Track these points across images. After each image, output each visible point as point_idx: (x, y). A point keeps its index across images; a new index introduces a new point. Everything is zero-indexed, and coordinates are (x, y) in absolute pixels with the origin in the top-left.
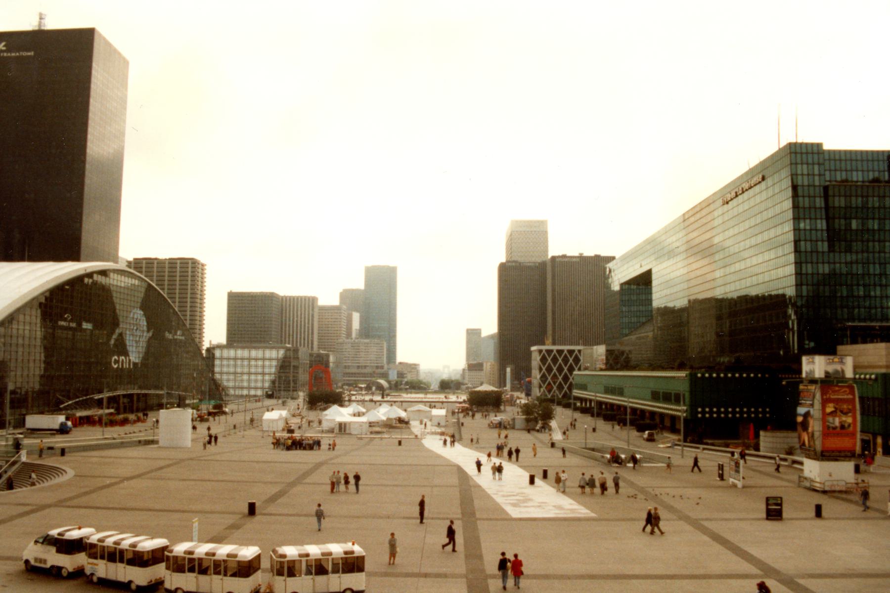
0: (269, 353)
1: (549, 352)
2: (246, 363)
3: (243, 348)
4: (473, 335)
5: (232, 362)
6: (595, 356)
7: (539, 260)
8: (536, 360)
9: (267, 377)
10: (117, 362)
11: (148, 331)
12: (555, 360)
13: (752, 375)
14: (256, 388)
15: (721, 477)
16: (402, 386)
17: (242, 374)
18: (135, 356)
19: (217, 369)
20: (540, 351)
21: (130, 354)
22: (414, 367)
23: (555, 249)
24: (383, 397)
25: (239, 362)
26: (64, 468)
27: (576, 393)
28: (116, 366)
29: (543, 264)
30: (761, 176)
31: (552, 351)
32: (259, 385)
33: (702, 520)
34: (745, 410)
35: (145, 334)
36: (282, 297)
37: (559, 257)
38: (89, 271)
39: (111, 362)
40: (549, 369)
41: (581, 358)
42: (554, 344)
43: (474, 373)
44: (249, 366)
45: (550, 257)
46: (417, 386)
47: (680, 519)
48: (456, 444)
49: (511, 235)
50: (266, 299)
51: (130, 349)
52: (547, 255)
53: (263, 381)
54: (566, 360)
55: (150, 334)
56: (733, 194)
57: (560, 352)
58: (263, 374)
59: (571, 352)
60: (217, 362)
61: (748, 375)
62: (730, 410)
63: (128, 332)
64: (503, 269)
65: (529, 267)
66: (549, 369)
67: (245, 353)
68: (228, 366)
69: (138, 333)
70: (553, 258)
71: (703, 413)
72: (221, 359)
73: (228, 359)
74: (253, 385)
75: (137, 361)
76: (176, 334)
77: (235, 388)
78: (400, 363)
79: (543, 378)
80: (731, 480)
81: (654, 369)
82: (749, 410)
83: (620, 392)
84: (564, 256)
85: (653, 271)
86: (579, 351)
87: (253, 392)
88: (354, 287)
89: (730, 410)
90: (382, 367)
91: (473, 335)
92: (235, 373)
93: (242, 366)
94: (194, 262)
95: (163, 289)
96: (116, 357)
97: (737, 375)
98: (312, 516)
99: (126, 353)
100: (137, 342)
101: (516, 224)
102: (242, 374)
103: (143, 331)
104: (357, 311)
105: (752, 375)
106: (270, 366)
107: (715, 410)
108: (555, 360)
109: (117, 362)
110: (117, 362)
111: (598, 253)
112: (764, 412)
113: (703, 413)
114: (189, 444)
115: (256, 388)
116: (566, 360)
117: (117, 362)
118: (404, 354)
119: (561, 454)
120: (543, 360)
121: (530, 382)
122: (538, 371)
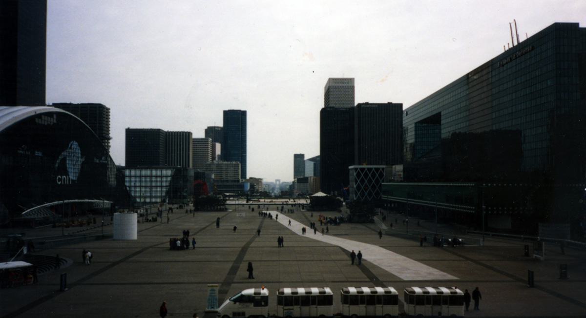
0: (165, 172)
1: (362, 169)
2: (148, 179)
3: (146, 169)
4: (299, 159)
5: (138, 179)
6: (394, 172)
7: (349, 106)
9: (164, 189)
10: (60, 180)
11: (82, 158)
12: (366, 175)
14: (156, 197)
15: (527, 254)
16: (255, 194)
17: (156, 187)
18: (73, 176)
19: (127, 184)
20: (356, 169)
21: (70, 174)
22: (258, 181)
23: (360, 98)
24: (247, 202)
25: (154, 179)
26: (64, 258)
27: (384, 197)
28: (59, 183)
30: (531, 47)
32: (159, 194)
34: (495, 208)
35: (80, 159)
36: (166, 132)
37: (363, 104)
39: (56, 180)
40: (362, 181)
41: (384, 174)
44: (151, 181)
45: (356, 104)
46: (266, 195)
48: (317, 232)
49: (329, 89)
50: (156, 133)
51: (69, 170)
52: (354, 104)
53: (161, 192)
54: (373, 175)
55: (83, 160)
56: (508, 59)
57: (370, 169)
58: (162, 187)
59: (377, 169)
60: (127, 179)
62: (511, 208)
63: (68, 158)
64: (324, 113)
69: (75, 158)
70: (359, 105)
72: (130, 176)
74: (154, 194)
75: (75, 179)
76: (101, 159)
77: (140, 197)
78: (251, 178)
79: (358, 188)
80: (535, 255)
84: (367, 104)
85: (442, 114)
86: (383, 169)
87: (154, 200)
88: (217, 125)
90: (238, 181)
91: (299, 159)
92: (151, 187)
93: (146, 181)
96: (60, 177)
99: (67, 174)
100: (74, 165)
101: (331, 80)
102: (156, 187)
103: (78, 157)
104: (218, 142)
106: (166, 181)
107: (500, 208)
108: (366, 175)
109: (61, 180)
110: (60, 180)
111: (390, 101)
114: (135, 236)
115: (156, 197)
116: (373, 175)
117: (61, 180)
119: (378, 236)
120: (358, 175)
121: (348, 191)
122: (354, 183)
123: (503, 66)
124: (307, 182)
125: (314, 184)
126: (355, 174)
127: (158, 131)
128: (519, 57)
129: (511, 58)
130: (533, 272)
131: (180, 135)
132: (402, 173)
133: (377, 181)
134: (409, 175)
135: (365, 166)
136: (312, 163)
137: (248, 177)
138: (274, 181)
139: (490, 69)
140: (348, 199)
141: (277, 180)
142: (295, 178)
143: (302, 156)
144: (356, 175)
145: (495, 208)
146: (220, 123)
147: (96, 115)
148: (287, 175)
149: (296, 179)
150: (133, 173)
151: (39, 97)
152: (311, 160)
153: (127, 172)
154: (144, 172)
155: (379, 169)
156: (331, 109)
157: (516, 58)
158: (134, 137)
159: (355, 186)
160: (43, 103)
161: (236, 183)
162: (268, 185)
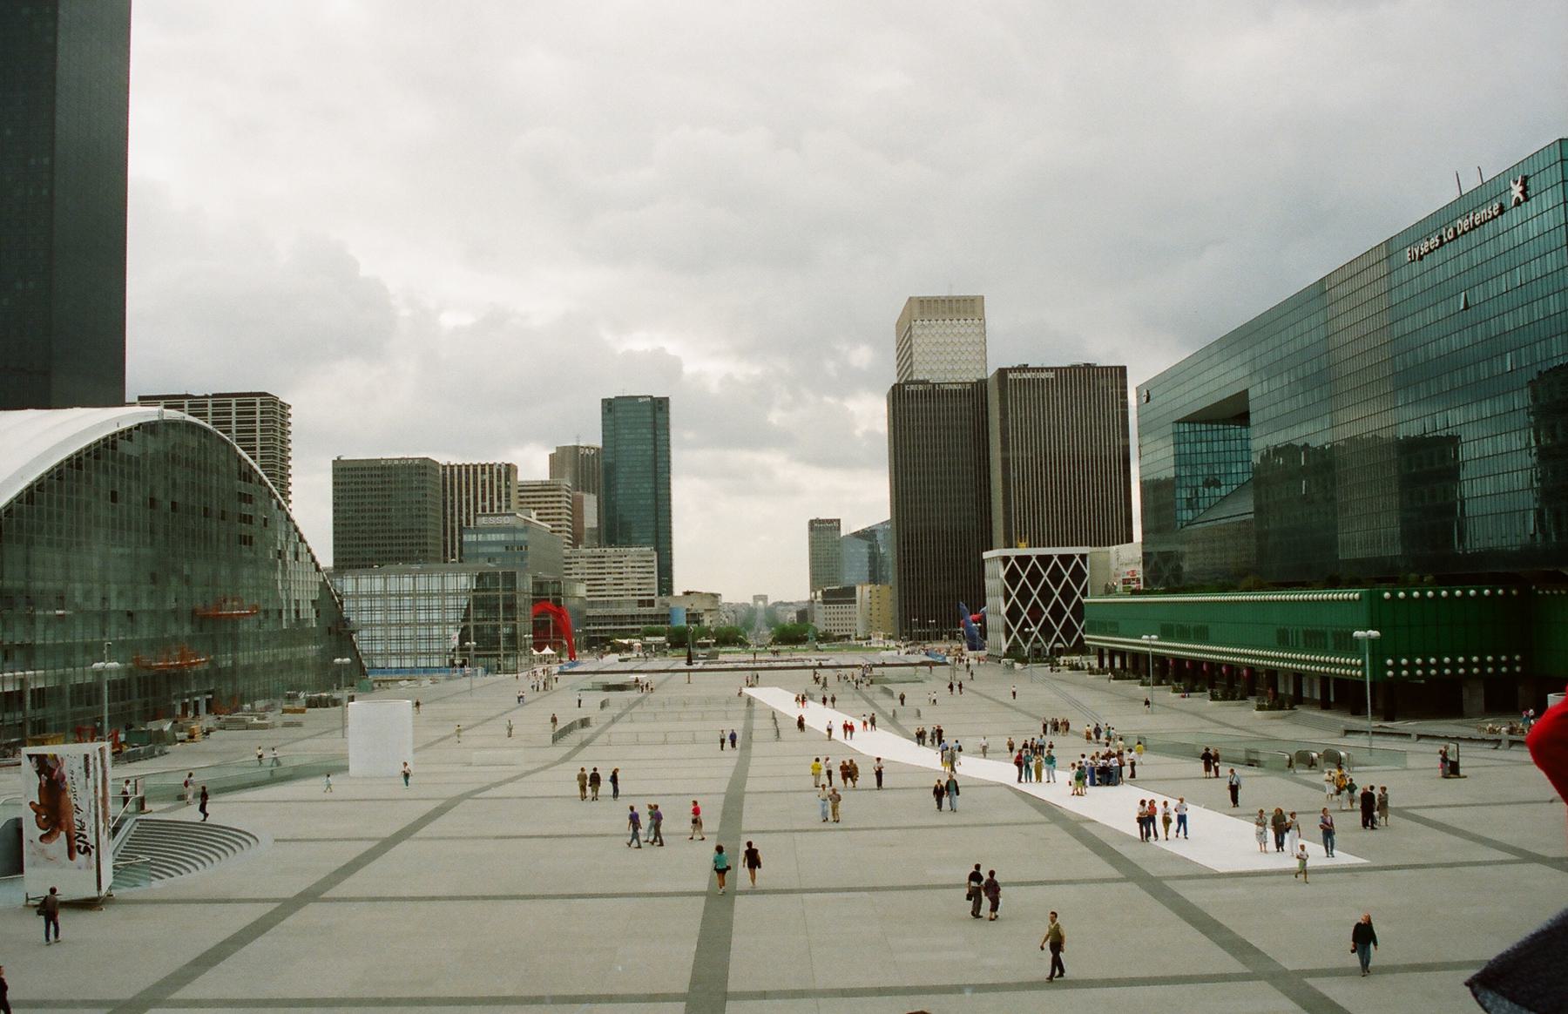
1: (1024, 560)
7: (973, 377)
8: (995, 578)
12: (1034, 577)
13: (1472, 592)
20: (1006, 560)
24: (689, 662)
25: (407, 602)
29: (982, 384)
30: (1496, 206)
31: (1028, 558)
33: (1118, 880)
38: (125, 425)
40: (1024, 595)
41: (1087, 571)
42: (1010, 546)
43: (833, 609)
45: (991, 371)
47: (1159, 880)
54: (1056, 577)
56: (1435, 240)
59: (1066, 559)
61: (1465, 593)
65: (952, 393)
66: (1024, 595)
67: (407, 583)
68: (429, 609)
71: (1397, 667)
72: (357, 596)
73: (429, 595)
77: (387, 654)
79: (1013, 614)
81: (1224, 589)
82: (1497, 659)
83: (1201, 635)
85: (1252, 394)
86: (1083, 557)
89: (1475, 659)
94: (269, 400)
95: (254, 458)
97: (1444, 593)
98: (1005, 884)
105: (1472, 592)
108: (1034, 577)
112: (1510, 663)
113: (1397, 667)
115: (429, 654)
116: (1056, 577)
118: (693, 571)
120: (1012, 576)
122: (1002, 600)
123: (1421, 258)
124: (854, 602)
125: (875, 606)
126: (1003, 574)
127: (424, 468)
128: (1464, 233)
129: (1441, 237)
130: (1365, 824)
131: (499, 472)
132: (1139, 569)
133: (1067, 594)
134: (1162, 571)
135: (1023, 551)
136: (863, 549)
137: (678, 591)
138: (750, 601)
139: (1383, 269)
140: (982, 648)
141: (756, 598)
142: (813, 589)
143: (834, 524)
144: (1007, 577)
145: (1404, 661)
146: (593, 438)
147: (259, 418)
148: (792, 585)
149: (819, 593)
150: (365, 583)
151: (110, 390)
152: (859, 535)
153: (348, 584)
154: (394, 584)
155: (1072, 557)
156: (921, 387)
157: (1456, 236)
158: (358, 484)
159: (1004, 610)
160: (110, 390)
161: (646, 610)
162: (734, 609)
